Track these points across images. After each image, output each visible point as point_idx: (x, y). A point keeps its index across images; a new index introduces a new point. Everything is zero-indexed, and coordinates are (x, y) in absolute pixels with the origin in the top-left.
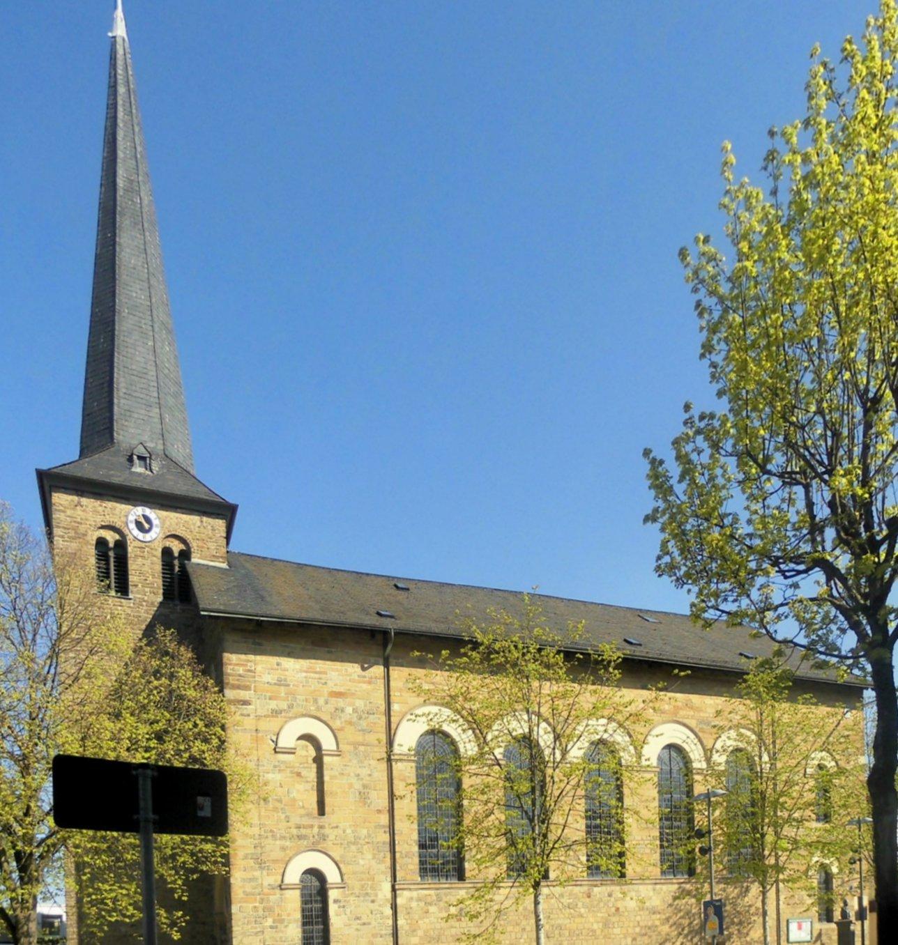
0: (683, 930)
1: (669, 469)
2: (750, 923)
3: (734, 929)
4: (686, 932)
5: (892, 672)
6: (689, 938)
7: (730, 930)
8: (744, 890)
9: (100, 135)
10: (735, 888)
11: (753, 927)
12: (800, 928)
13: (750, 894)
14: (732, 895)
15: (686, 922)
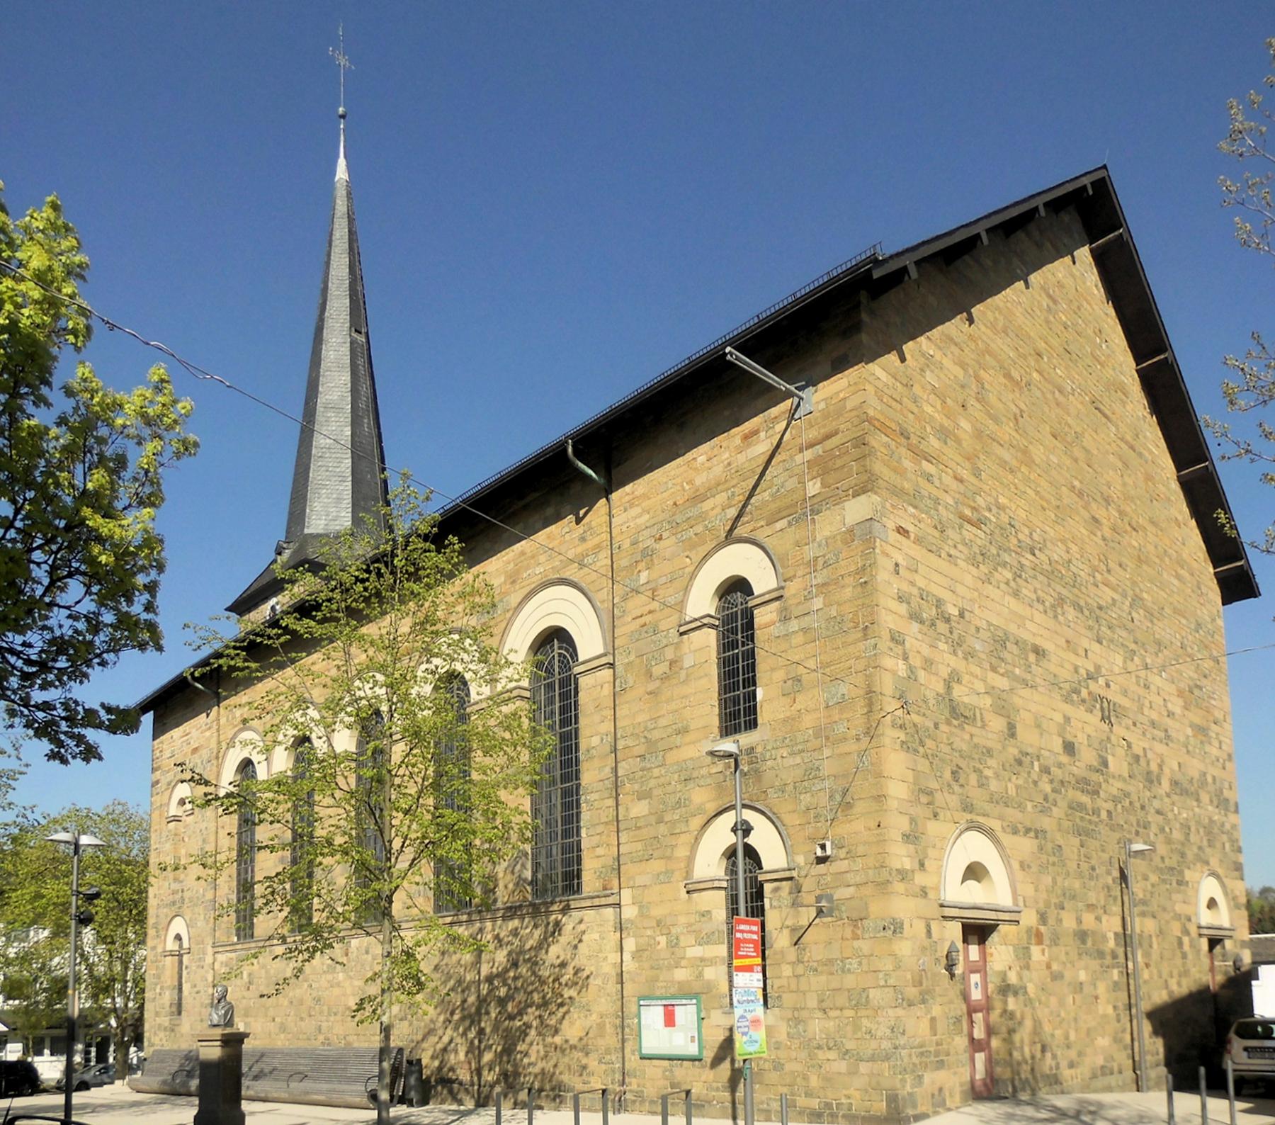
0: (452, 1013)
1: (1244, 850)
2: (562, 1005)
3: (531, 1016)
4: (456, 1017)
5: (1251, 991)
6: (461, 1030)
7: (525, 1018)
8: (551, 928)
9: (312, 329)
10: (536, 926)
11: (567, 1012)
12: (670, 1020)
13: (562, 939)
14: (531, 943)
15: (457, 999)
